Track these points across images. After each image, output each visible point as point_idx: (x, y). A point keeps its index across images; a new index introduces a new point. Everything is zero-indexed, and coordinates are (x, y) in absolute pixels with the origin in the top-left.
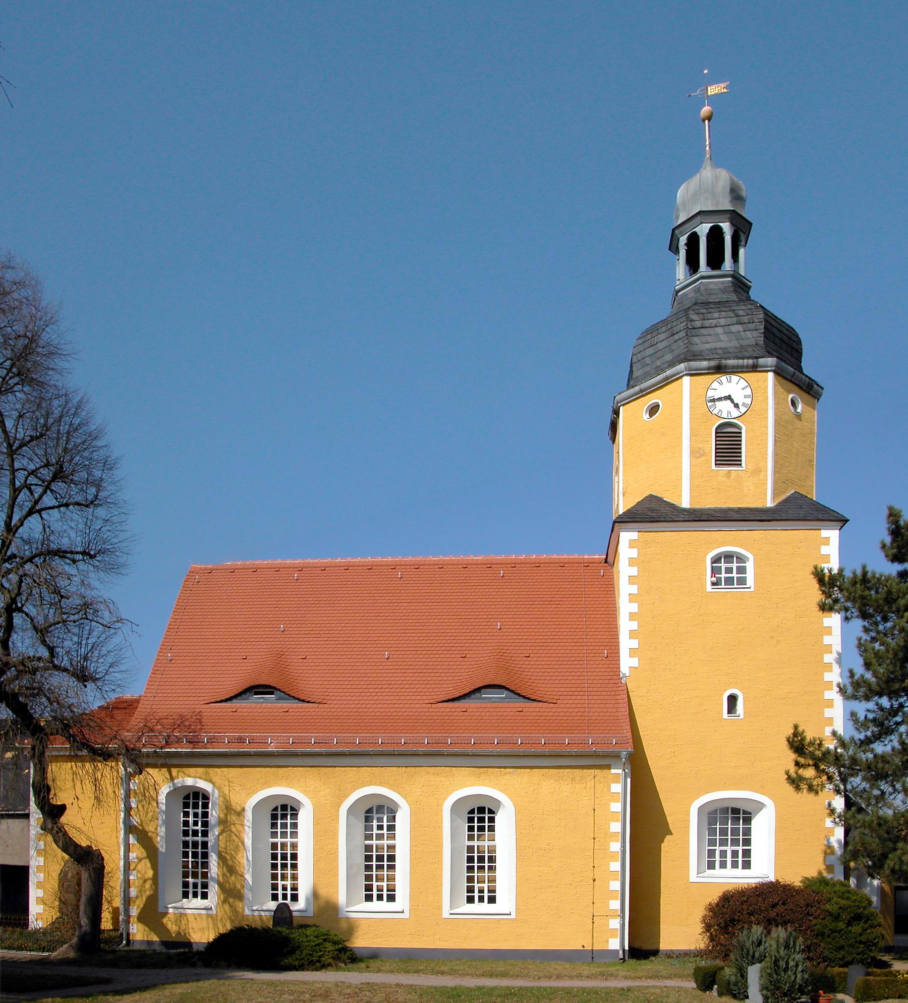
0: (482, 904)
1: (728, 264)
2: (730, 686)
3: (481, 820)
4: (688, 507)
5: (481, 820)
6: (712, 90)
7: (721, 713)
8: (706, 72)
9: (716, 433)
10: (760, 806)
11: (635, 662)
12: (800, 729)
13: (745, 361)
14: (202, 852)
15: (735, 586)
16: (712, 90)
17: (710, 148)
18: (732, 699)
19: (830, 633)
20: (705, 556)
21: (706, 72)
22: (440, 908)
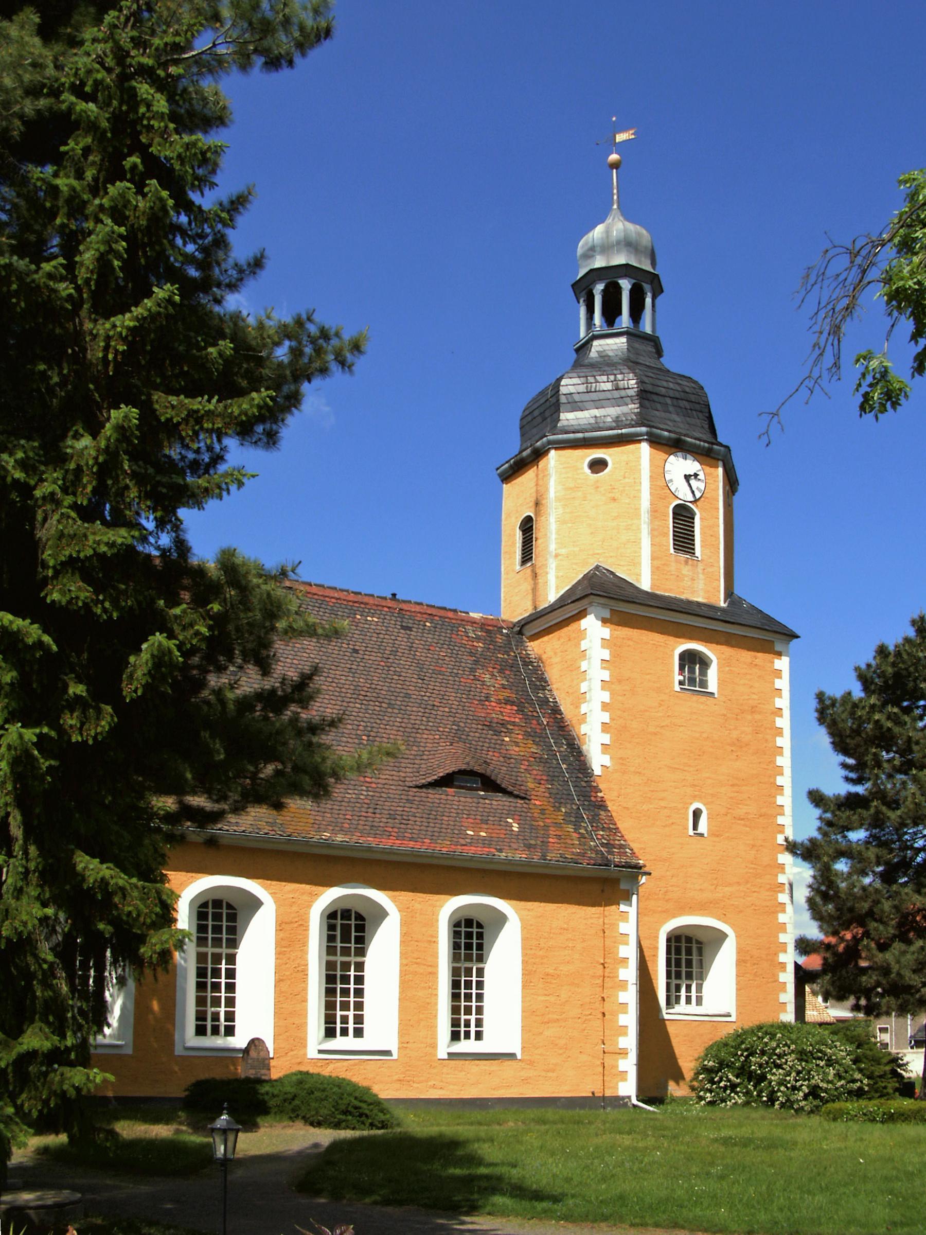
0: (467, 1041)
1: (625, 319)
2: (695, 798)
3: (469, 935)
4: (649, 590)
5: (469, 935)
6: (621, 137)
7: (687, 829)
8: (614, 119)
9: (674, 513)
10: (723, 936)
11: (606, 760)
12: (319, 681)
13: (702, 443)
14: (226, 983)
15: (697, 689)
16: (621, 137)
17: (618, 197)
18: (697, 814)
19: (781, 754)
20: (673, 651)
21: (614, 119)
22: (434, 1046)
